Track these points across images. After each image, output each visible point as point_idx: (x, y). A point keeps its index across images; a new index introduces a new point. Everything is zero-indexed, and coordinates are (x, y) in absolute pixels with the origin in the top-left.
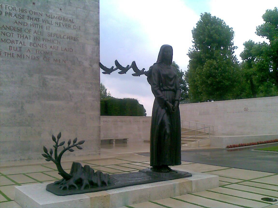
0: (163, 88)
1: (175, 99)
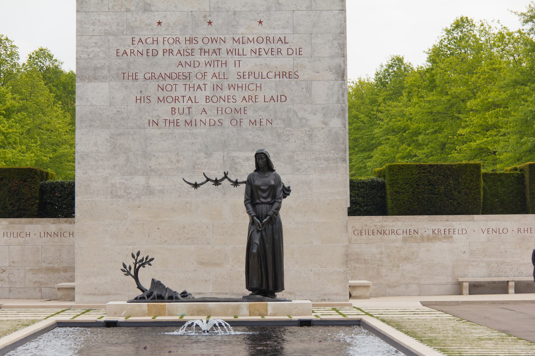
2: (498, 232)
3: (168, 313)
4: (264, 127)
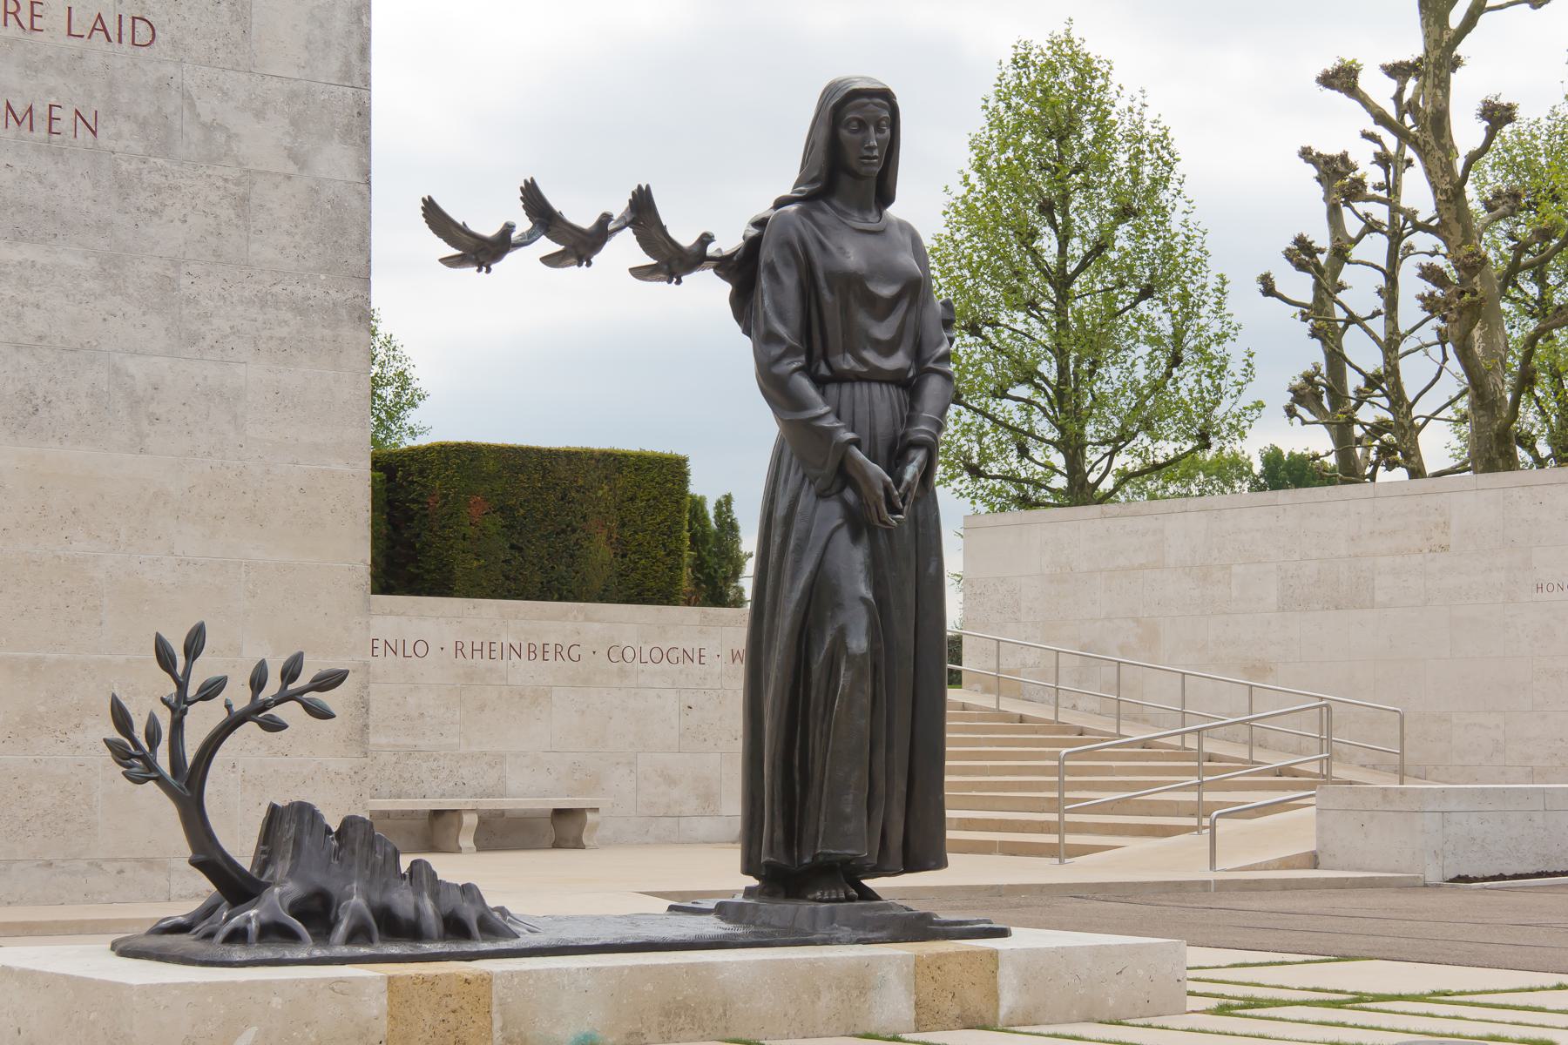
0: (829, 366)
1: (904, 436)
2: (400, 652)
3: (503, 1029)
4: (64, 141)
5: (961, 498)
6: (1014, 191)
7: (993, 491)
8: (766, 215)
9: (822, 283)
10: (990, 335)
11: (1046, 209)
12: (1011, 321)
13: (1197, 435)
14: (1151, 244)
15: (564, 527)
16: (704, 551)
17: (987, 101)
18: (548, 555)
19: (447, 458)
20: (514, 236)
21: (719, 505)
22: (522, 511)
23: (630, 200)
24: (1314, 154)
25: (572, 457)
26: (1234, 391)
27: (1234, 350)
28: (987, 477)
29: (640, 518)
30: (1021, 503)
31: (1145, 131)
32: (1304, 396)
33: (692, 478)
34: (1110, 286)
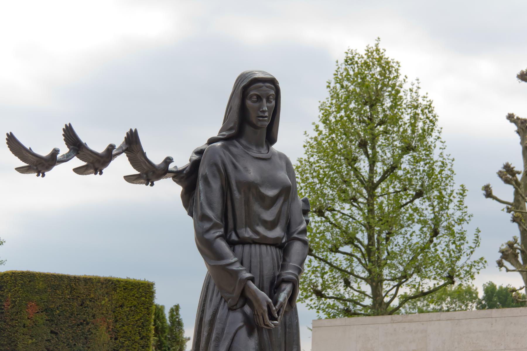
5: (311, 309)
6: (345, 134)
7: (329, 306)
8: (203, 148)
9: (234, 187)
10: (329, 216)
11: (363, 145)
12: (341, 208)
13: (447, 277)
14: (421, 166)
15: (82, 321)
16: (163, 337)
17: (330, 83)
18: (72, 337)
19: (16, 280)
20: (59, 156)
21: (172, 311)
22: (58, 312)
23: (125, 138)
24: (515, 118)
25: (87, 281)
26: (469, 252)
27: (470, 230)
28: (326, 298)
29: (126, 317)
30: (345, 313)
31: (419, 102)
32: (508, 255)
33: (157, 295)
34: (398, 190)
